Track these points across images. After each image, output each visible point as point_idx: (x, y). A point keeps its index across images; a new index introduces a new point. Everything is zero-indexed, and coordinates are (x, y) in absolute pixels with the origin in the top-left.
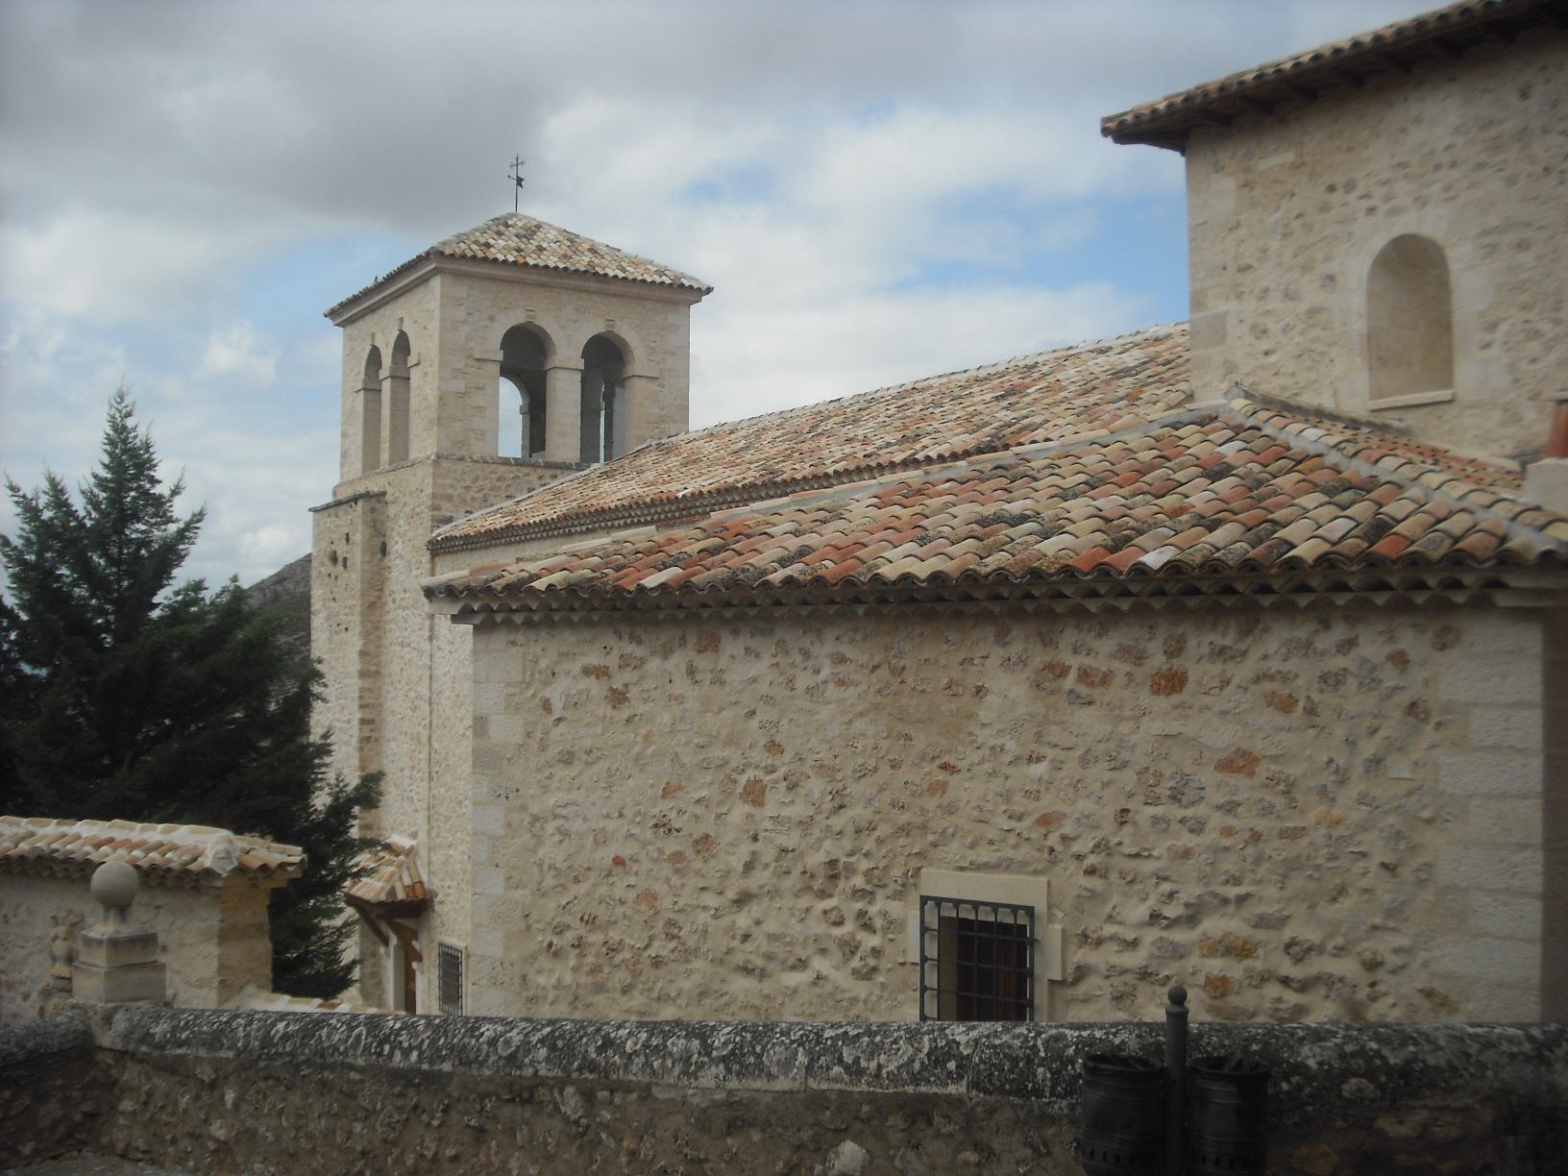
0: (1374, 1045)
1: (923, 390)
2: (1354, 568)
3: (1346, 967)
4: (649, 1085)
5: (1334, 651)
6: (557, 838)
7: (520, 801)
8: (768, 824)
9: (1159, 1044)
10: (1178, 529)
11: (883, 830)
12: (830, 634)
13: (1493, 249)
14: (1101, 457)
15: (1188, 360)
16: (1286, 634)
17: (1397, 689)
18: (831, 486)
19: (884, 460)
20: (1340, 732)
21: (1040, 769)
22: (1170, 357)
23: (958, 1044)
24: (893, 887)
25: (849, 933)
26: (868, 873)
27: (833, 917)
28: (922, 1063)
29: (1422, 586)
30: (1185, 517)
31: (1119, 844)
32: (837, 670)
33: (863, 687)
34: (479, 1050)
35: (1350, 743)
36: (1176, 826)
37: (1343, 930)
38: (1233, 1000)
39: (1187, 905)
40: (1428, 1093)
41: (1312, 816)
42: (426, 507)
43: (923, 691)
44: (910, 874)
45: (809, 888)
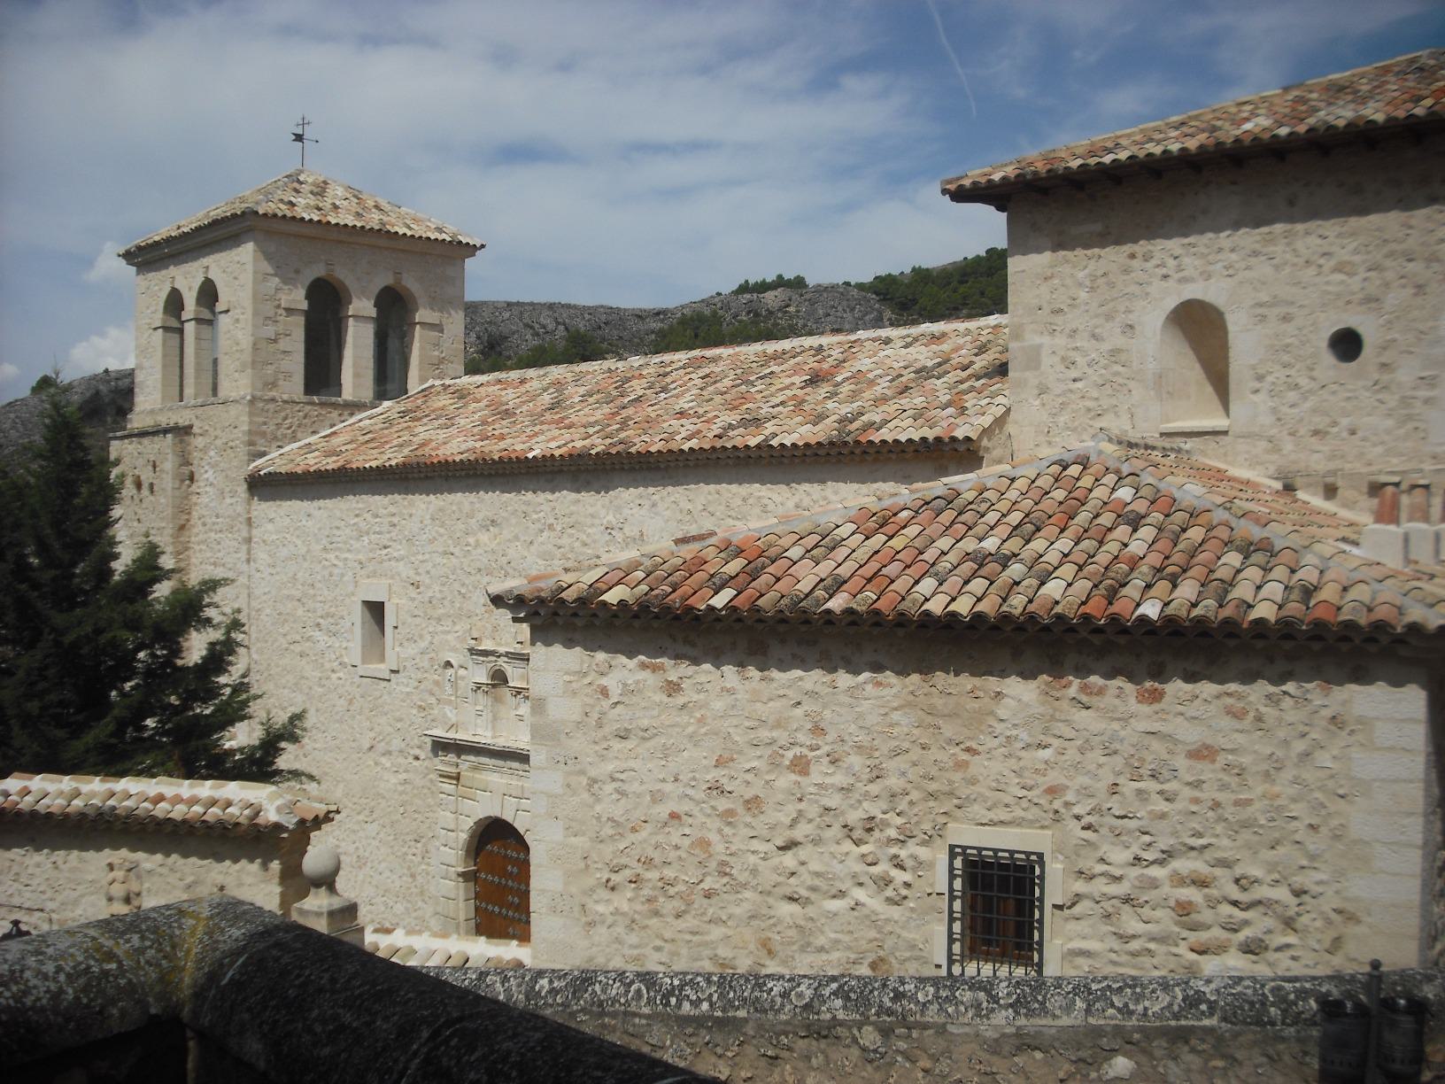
3: (1282, 894)
4: (945, 1024)
6: (615, 796)
7: (578, 767)
8: (812, 789)
21: (1046, 754)
23: (1204, 993)
28: (1180, 1006)
34: (773, 1001)
36: (1155, 797)
42: (242, 442)
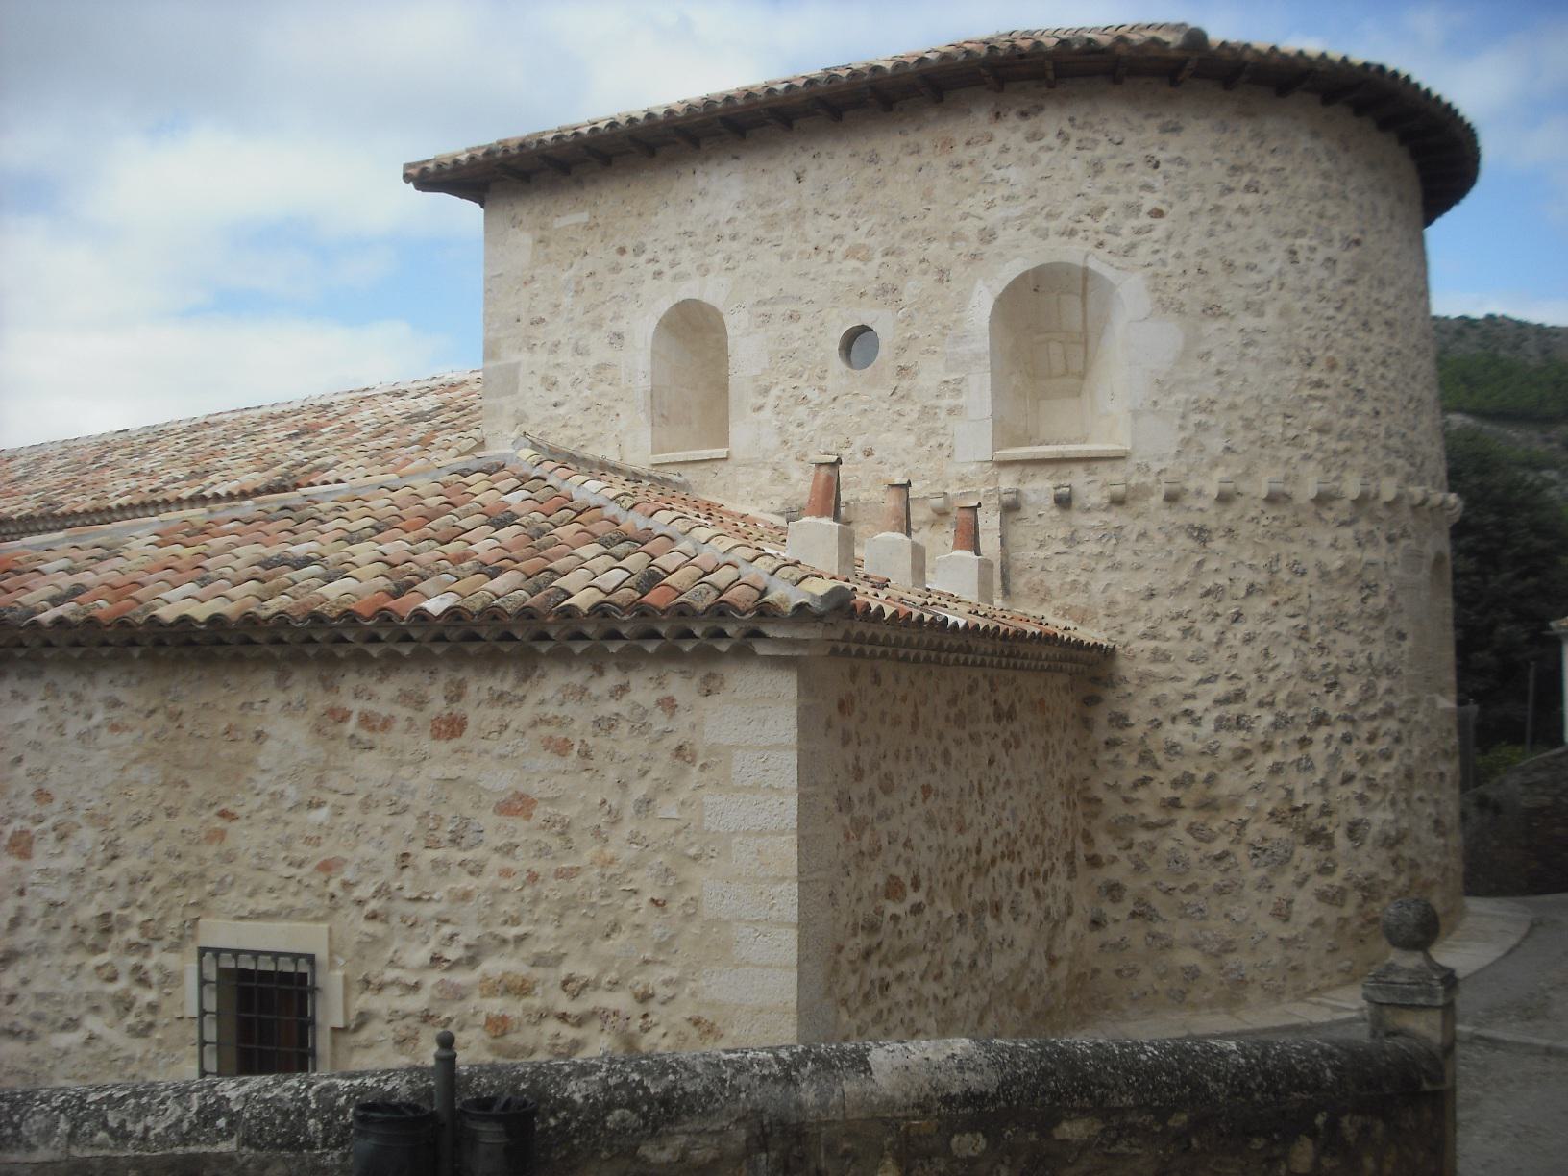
0: (636, 1077)
1: (215, 425)
2: (626, 617)
3: (621, 1001)
5: (607, 696)
8: (35, 878)
9: (430, 1088)
10: (460, 574)
11: (159, 881)
12: (103, 677)
13: (767, 318)
14: (389, 502)
15: (481, 408)
16: (563, 681)
17: (666, 732)
18: (158, 513)
19: (170, 496)
20: (612, 775)
21: (321, 815)
22: (465, 404)
24: (170, 939)
25: (122, 990)
26: (143, 927)
27: (106, 972)
28: (191, 1122)
29: (689, 635)
30: (467, 564)
31: (400, 888)
32: (110, 715)
33: (137, 733)
35: (622, 785)
36: (455, 869)
37: (617, 965)
38: (514, 1038)
39: (468, 947)
40: (686, 1118)
41: (587, 856)
43: (201, 736)
44: (187, 925)
45: (80, 943)
